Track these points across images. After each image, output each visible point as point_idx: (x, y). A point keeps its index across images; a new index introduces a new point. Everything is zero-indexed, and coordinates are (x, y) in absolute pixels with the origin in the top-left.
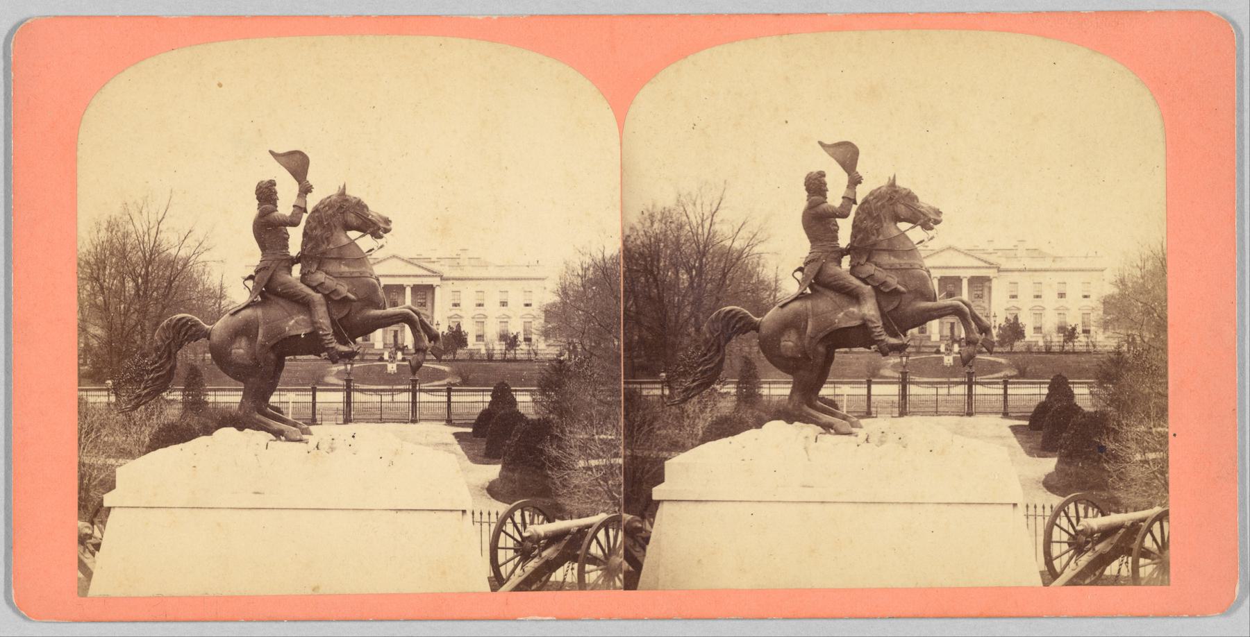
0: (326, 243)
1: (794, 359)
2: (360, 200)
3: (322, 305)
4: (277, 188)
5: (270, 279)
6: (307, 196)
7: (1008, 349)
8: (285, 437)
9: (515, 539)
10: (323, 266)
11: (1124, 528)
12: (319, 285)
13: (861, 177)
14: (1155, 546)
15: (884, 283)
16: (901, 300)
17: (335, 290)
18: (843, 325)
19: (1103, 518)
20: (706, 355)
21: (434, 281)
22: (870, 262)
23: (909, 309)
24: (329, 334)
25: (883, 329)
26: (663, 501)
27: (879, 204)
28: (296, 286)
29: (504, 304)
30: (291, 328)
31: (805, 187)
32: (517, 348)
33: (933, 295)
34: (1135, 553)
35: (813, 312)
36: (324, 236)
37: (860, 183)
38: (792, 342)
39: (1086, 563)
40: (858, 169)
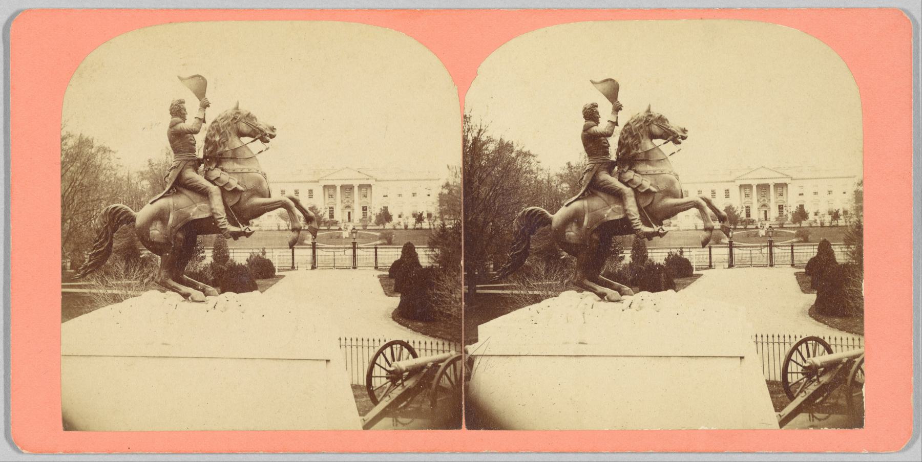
0: (635, 149)
1: (576, 245)
2: (661, 116)
3: (218, 195)
6: (618, 113)
11: (842, 364)
12: (628, 181)
17: (641, 185)
18: (196, 217)
19: (415, 359)
21: (787, 181)
22: (631, 170)
23: (247, 204)
26: (477, 355)
27: (638, 125)
37: (621, 109)
38: (158, 230)
40: (619, 99)
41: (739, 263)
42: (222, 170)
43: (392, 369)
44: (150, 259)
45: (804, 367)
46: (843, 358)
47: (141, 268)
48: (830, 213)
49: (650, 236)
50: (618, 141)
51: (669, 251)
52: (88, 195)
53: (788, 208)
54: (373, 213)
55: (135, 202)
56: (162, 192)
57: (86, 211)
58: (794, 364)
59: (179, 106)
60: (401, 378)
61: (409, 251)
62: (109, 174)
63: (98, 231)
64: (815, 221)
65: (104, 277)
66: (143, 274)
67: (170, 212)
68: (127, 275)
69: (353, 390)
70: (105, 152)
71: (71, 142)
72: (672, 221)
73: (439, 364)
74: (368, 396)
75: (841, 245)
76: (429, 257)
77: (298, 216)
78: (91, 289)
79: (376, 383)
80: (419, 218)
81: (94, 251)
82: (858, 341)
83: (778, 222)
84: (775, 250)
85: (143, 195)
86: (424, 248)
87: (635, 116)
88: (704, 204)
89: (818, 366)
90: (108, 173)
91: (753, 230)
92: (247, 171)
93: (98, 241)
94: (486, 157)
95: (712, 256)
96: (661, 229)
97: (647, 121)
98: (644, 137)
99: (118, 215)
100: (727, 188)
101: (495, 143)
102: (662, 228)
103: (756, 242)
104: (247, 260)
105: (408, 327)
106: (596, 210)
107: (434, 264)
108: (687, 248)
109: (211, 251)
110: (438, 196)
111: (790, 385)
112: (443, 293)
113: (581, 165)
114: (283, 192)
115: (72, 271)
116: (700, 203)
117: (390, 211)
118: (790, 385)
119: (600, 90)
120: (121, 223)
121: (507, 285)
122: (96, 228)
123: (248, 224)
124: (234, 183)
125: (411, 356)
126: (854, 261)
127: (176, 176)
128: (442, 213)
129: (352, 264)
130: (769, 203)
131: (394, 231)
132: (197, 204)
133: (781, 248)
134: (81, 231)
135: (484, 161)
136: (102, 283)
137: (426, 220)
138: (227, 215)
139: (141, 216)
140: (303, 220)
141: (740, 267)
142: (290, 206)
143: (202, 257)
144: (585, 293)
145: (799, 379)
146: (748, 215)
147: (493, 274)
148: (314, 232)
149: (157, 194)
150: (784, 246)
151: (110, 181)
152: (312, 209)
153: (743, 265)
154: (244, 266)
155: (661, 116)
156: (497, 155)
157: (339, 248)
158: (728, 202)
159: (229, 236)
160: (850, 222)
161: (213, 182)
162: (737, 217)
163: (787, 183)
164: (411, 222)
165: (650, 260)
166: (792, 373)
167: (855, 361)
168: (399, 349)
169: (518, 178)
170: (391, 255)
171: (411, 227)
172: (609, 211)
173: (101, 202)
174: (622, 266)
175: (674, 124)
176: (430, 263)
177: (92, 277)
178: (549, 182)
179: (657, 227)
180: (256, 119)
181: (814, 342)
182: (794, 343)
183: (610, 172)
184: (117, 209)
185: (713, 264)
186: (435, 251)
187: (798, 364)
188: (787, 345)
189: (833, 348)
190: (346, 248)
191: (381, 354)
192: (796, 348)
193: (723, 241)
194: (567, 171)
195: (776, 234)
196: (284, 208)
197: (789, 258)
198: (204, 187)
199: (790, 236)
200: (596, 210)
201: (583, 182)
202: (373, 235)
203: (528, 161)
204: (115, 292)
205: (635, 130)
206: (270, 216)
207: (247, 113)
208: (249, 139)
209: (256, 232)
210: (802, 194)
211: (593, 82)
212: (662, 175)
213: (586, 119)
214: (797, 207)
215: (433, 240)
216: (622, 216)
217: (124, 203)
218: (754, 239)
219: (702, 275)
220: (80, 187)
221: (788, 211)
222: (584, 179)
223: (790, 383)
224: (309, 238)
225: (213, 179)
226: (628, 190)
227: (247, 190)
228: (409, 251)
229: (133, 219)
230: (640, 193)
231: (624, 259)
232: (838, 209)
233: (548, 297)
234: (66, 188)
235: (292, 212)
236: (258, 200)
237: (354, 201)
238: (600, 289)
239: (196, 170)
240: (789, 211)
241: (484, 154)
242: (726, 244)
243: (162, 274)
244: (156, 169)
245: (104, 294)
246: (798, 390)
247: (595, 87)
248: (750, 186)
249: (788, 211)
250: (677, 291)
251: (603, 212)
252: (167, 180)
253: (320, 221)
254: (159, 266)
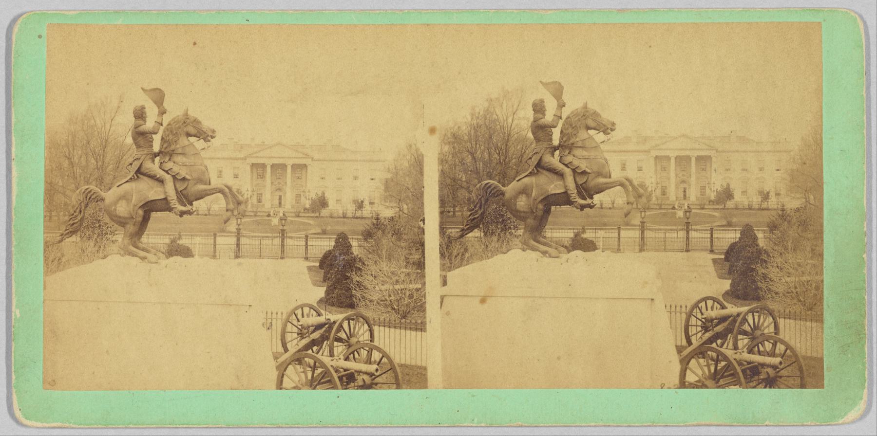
4: (545, 104)
5: (540, 160)
7: (317, 214)
8: (549, 255)
9: (298, 328)
14: (749, 328)
16: (588, 178)
18: (553, 192)
20: (473, 209)
28: (555, 164)
32: (769, 200)
34: (735, 331)
39: (707, 338)
42: (574, 156)
58: (693, 318)
98: (582, 128)
99: (490, 189)
116: (224, 190)
124: (183, 173)
130: (284, 187)
138: (578, 191)
155: (595, 112)
161: (566, 165)
166: (692, 326)
172: (152, 192)
180: (600, 116)
184: (489, 184)
198: (560, 169)
212: (195, 167)
227: (193, 179)
236: (602, 180)
237: (286, 183)
240: (713, 190)
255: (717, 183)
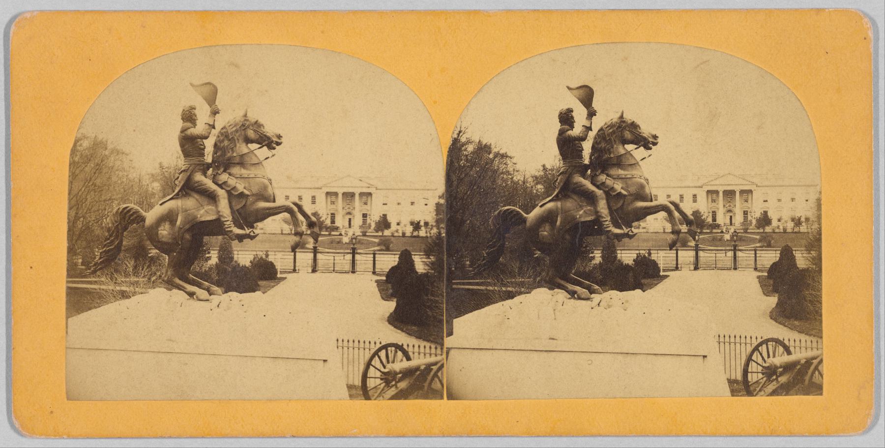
2: (633, 122)
3: (224, 198)
6: (593, 118)
10: (228, 169)
11: (419, 371)
13: (596, 111)
15: (234, 188)
18: (203, 219)
22: (603, 173)
24: (228, 221)
25: (610, 223)
26: (452, 348)
27: (611, 131)
29: (779, 200)
30: (581, 216)
31: (559, 120)
33: (650, 197)
35: (182, 208)
36: (607, 148)
37: (595, 115)
38: (167, 231)
40: (593, 105)
41: (704, 266)
42: (230, 174)
43: (386, 370)
44: (158, 258)
45: (763, 367)
46: (800, 360)
47: (149, 266)
48: (793, 220)
49: (619, 237)
50: (591, 145)
51: (638, 252)
52: (101, 195)
53: (753, 214)
54: (373, 220)
55: (145, 203)
56: (171, 194)
57: (98, 210)
58: (754, 364)
59: (190, 112)
60: (394, 379)
61: (406, 258)
62: (121, 175)
63: (109, 230)
64: (778, 227)
65: (113, 274)
66: (150, 273)
67: (178, 213)
68: (136, 273)
69: (348, 390)
70: (117, 154)
71: (86, 144)
72: (641, 223)
73: (432, 367)
74: (362, 396)
75: (802, 250)
76: (425, 263)
77: (301, 221)
78: (100, 285)
79: (371, 383)
80: (416, 226)
81: (104, 249)
82: (816, 343)
83: (741, 227)
84: (739, 254)
85: (153, 197)
86: (419, 255)
87: (609, 122)
88: (672, 208)
89: (777, 367)
90: (121, 173)
91: (718, 234)
92: (254, 176)
93: (109, 239)
94: (465, 158)
95: (679, 258)
96: (630, 231)
97: (619, 127)
100: (694, 193)
101: (473, 144)
102: (631, 230)
103: (721, 246)
104: (251, 262)
105: (402, 331)
106: (569, 211)
107: (430, 271)
108: (655, 250)
109: (216, 252)
110: (435, 205)
111: (750, 384)
112: (437, 299)
113: (555, 168)
114: (287, 197)
115: (83, 267)
117: (389, 218)
118: (750, 384)
119: (575, 96)
120: (133, 222)
121: (482, 281)
122: (107, 226)
123: (252, 227)
124: (241, 187)
125: (404, 359)
126: (814, 267)
127: (185, 179)
128: (438, 222)
129: (351, 269)
131: (392, 238)
132: (205, 207)
133: (744, 252)
134: (93, 229)
135: (463, 161)
136: (111, 279)
137: (423, 228)
139: (150, 217)
140: (305, 224)
141: (705, 269)
142: (293, 211)
143: (208, 257)
144: (556, 290)
145: (759, 378)
146: (714, 219)
147: (469, 270)
148: (316, 237)
149: (167, 196)
150: (747, 250)
151: (123, 182)
152: (315, 214)
153: (708, 268)
154: (248, 268)
155: (633, 122)
156: (475, 156)
157: (338, 253)
158: (696, 206)
159: (234, 237)
160: (811, 229)
161: (220, 186)
162: (703, 221)
163: (753, 190)
164: (409, 230)
165: (619, 261)
167: (813, 363)
168: (393, 352)
169: (495, 179)
170: (388, 261)
171: (408, 234)
172: (581, 212)
173: (112, 202)
174: (592, 265)
175: (646, 130)
176: (426, 270)
177: (102, 274)
178: (524, 183)
179: (627, 229)
181: (774, 343)
182: (755, 343)
183: (584, 175)
184: (128, 208)
185: (679, 266)
186: (431, 259)
187: (758, 364)
188: (748, 346)
189: (792, 349)
190: (346, 253)
191: (376, 356)
192: (756, 349)
193: (690, 244)
194: (542, 173)
195: (741, 239)
196: (288, 213)
197: (753, 262)
199: (753, 241)
200: (569, 211)
201: (557, 184)
202: (372, 241)
203: (504, 162)
204: (124, 288)
205: (608, 135)
206: (274, 220)
207: (255, 120)
208: (257, 146)
209: (260, 235)
210: (767, 201)
211: (569, 88)
213: (561, 124)
214: (761, 213)
215: (429, 247)
216: (593, 218)
217: (134, 204)
218: (718, 243)
219: (669, 276)
220: (93, 186)
221: (752, 217)
222: (558, 181)
223: (750, 382)
224: (309, 242)
225: (220, 183)
226: (599, 192)
227: (253, 195)
228: (406, 258)
229: (143, 219)
230: (611, 196)
231: (594, 259)
232: (801, 216)
233: (520, 293)
234: (80, 188)
235: (295, 217)
236: (263, 204)
238: (571, 287)
239: (205, 174)
240: (753, 217)
241: (463, 155)
242: (691, 247)
243: (169, 273)
244: (167, 172)
245: (113, 290)
246: (758, 389)
247: (571, 92)
248: (717, 192)
249: (752, 217)
250: (644, 291)
251: (575, 214)
252: (177, 182)
253: (321, 225)
254: (167, 265)
255: (756, 213)
